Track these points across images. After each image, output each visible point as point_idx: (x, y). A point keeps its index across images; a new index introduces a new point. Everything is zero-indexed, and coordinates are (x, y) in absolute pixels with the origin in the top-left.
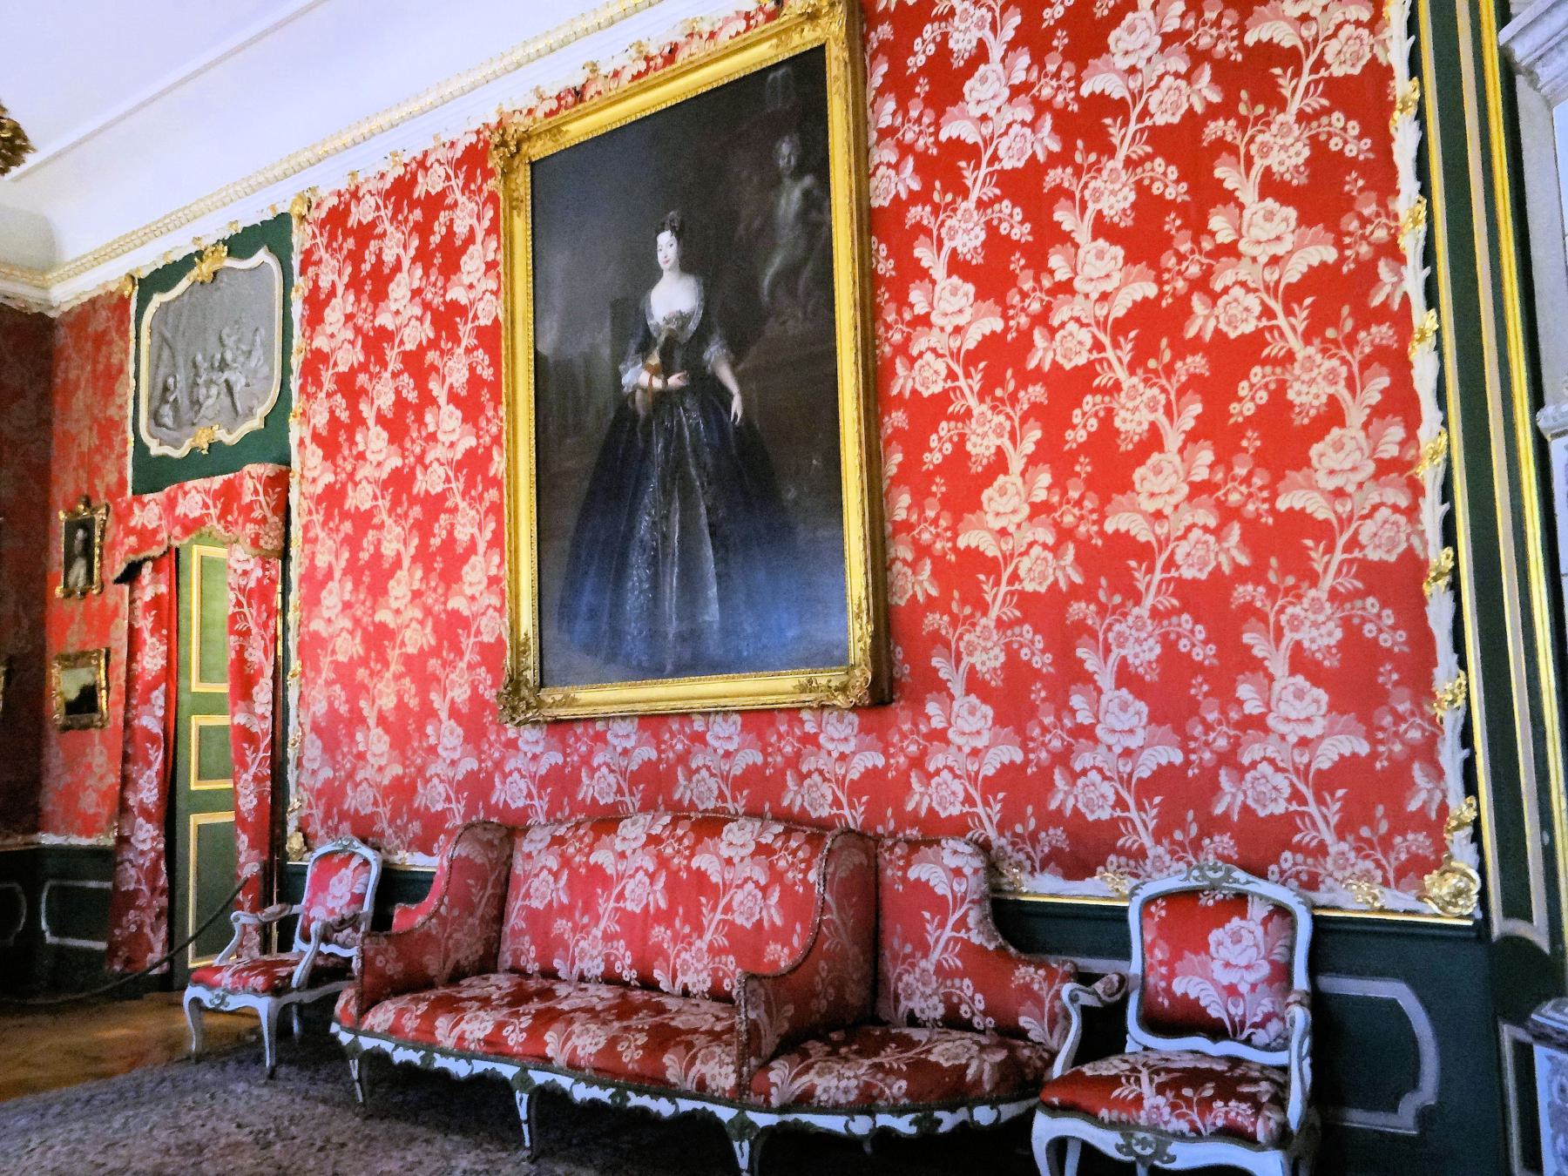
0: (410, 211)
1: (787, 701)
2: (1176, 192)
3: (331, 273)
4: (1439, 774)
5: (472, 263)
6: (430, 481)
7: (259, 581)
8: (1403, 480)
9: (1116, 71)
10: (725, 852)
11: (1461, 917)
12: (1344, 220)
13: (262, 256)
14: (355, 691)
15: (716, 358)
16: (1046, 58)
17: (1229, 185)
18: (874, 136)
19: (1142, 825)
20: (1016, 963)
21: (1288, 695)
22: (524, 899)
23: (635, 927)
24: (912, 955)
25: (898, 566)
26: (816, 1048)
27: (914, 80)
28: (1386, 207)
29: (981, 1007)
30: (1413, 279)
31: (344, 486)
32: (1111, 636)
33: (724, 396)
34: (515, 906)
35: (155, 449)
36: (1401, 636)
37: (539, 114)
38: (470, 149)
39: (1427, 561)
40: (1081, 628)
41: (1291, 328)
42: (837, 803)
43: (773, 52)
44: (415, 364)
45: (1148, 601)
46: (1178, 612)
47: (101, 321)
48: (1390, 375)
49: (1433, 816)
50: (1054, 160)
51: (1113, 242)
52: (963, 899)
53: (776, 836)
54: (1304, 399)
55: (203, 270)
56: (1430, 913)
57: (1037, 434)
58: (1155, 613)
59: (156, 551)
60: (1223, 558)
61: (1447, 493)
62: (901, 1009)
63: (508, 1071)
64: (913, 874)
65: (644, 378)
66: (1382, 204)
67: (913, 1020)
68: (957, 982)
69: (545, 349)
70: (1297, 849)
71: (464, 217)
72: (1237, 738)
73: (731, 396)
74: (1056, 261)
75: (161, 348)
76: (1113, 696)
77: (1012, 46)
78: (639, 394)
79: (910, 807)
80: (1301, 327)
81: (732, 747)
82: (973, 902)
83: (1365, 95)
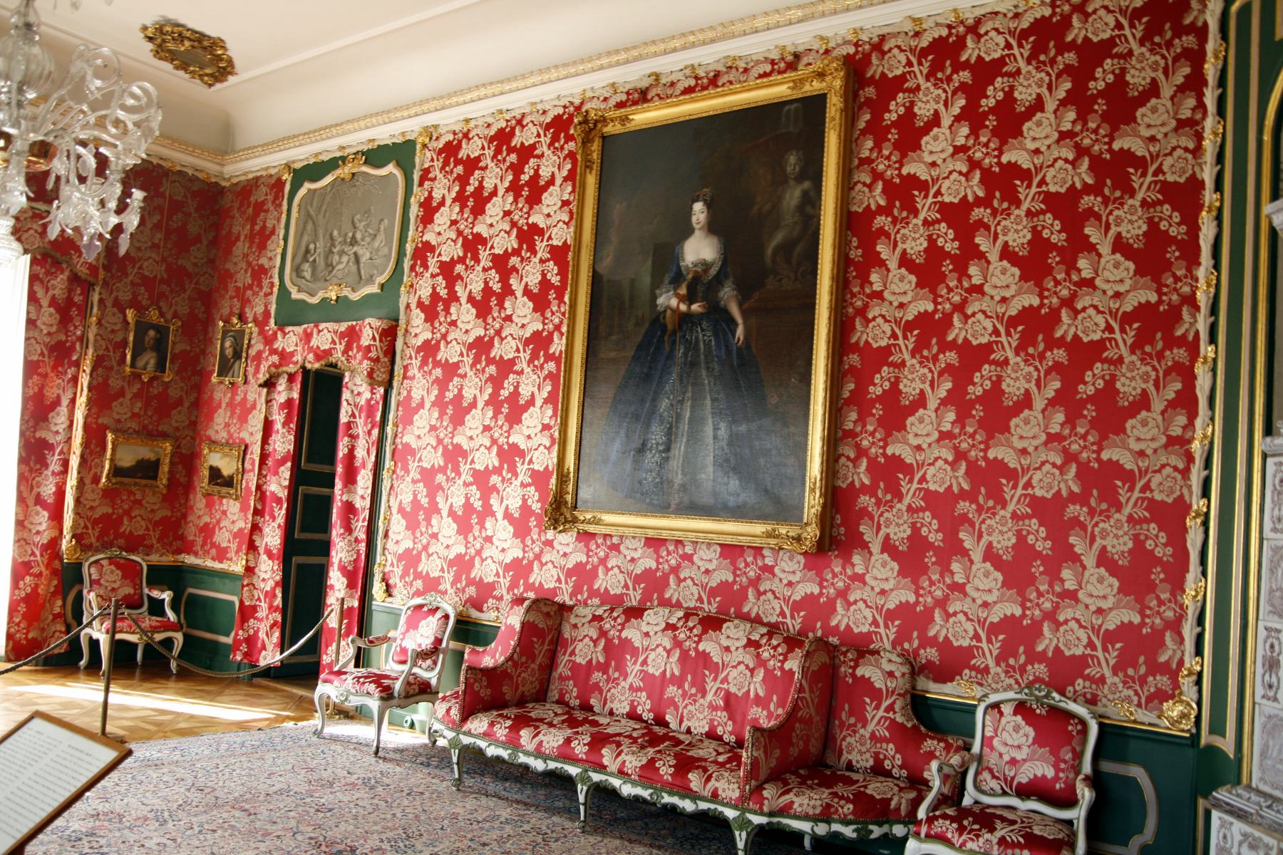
0: (508, 154)
1: (757, 542)
2: (1058, 238)
3: (443, 188)
4: (1182, 640)
5: (551, 199)
6: (450, 353)
7: (368, 401)
8: (1182, 451)
9: (1026, 150)
10: (645, 628)
11: (1183, 731)
12: (1164, 276)
13: (391, 168)
14: (487, 491)
15: (728, 296)
16: (1089, 117)
17: (983, 248)
18: (856, 162)
19: (989, 652)
20: (924, 737)
21: (1094, 580)
22: (722, 682)
23: (655, 685)
24: (855, 725)
25: (843, 460)
26: (793, 779)
27: (887, 129)
28: (1191, 272)
29: (899, 763)
30: (1202, 325)
31: (438, 342)
32: (1097, 530)
33: (732, 322)
34: (563, 659)
35: (295, 295)
36: (1169, 550)
37: (612, 102)
38: (558, 118)
39: (1190, 506)
40: (964, 519)
41: (1123, 341)
42: (782, 614)
43: (789, 92)
44: (500, 263)
45: (1011, 507)
46: (1029, 517)
47: (261, 194)
48: (1062, 381)
49: (1174, 666)
50: (979, 202)
51: (1127, 258)
52: (893, 692)
53: (762, 635)
54: (1126, 389)
55: (344, 171)
56: (1164, 726)
57: (949, 385)
58: (1014, 516)
59: (292, 368)
60: (1063, 486)
61: (1208, 464)
62: (843, 758)
63: (573, 770)
64: (859, 672)
65: (674, 302)
66: (1189, 270)
67: (850, 766)
68: (884, 745)
69: (600, 270)
70: (1086, 678)
71: (549, 165)
72: (1058, 603)
73: (737, 325)
74: (973, 270)
75: (305, 223)
76: (980, 566)
77: (957, 119)
78: (669, 312)
79: (833, 623)
80: (1129, 342)
81: (711, 567)
82: (899, 695)
83: (1185, 197)
